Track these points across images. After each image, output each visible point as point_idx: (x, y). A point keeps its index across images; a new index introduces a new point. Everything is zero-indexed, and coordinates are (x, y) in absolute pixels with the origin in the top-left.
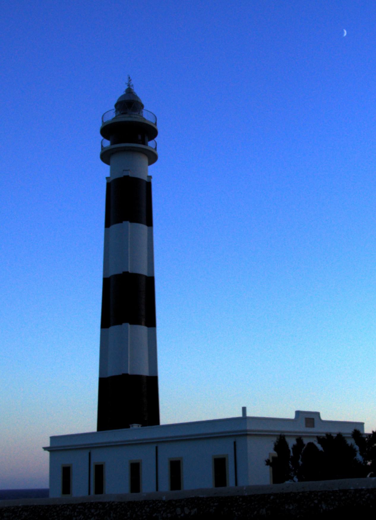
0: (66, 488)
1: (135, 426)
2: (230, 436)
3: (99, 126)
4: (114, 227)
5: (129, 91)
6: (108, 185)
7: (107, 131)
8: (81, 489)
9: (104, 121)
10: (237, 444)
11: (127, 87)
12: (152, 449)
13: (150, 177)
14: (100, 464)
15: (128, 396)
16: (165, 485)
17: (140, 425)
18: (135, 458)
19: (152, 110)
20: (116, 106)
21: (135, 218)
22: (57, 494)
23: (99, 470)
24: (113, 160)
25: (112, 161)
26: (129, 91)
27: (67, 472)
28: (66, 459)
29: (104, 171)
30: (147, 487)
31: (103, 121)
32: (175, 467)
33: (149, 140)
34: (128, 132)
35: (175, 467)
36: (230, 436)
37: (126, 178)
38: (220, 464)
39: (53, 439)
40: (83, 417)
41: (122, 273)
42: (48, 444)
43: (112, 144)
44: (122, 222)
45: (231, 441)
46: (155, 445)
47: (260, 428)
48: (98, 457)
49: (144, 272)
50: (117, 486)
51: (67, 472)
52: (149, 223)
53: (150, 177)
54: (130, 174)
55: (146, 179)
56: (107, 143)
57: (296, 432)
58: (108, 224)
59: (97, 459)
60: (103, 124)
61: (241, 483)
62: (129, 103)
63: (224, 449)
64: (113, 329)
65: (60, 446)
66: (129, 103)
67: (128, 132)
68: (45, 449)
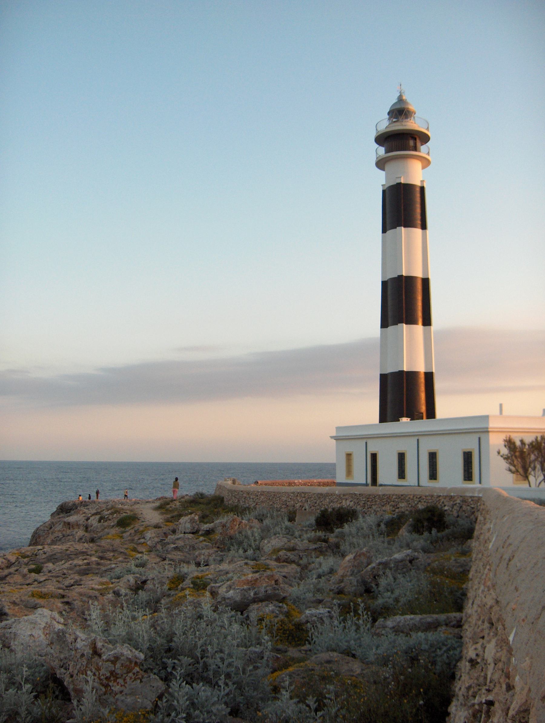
1: (405, 420)
2: (475, 432)
3: (373, 135)
4: (390, 232)
5: (400, 100)
6: (384, 192)
7: (383, 139)
8: (360, 475)
9: (379, 130)
10: (420, 441)
11: (399, 94)
12: (414, 441)
14: (468, 451)
17: (409, 419)
20: (389, 113)
21: (409, 223)
23: (374, 457)
24: (387, 167)
25: (386, 168)
26: (400, 100)
27: (349, 456)
28: (349, 447)
29: (379, 180)
31: (377, 129)
33: (422, 145)
34: (400, 140)
36: (475, 432)
37: (399, 185)
39: (338, 429)
41: (397, 276)
42: (334, 434)
43: (387, 152)
44: (396, 228)
45: (364, 441)
46: (476, 436)
49: (419, 273)
50: (387, 474)
51: (349, 456)
52: (424, 227)
54: (402, 181)
55: (418, 184)
56: (382, 151)
57: (541, 429)
58: (384, 231)
59: (372, 449)
60: (377, 133)
62: (400, 112)
63: (471, 444)
64: (391, 329)
66: (400, 112)
67: (400, 140)
68: (332, 437)
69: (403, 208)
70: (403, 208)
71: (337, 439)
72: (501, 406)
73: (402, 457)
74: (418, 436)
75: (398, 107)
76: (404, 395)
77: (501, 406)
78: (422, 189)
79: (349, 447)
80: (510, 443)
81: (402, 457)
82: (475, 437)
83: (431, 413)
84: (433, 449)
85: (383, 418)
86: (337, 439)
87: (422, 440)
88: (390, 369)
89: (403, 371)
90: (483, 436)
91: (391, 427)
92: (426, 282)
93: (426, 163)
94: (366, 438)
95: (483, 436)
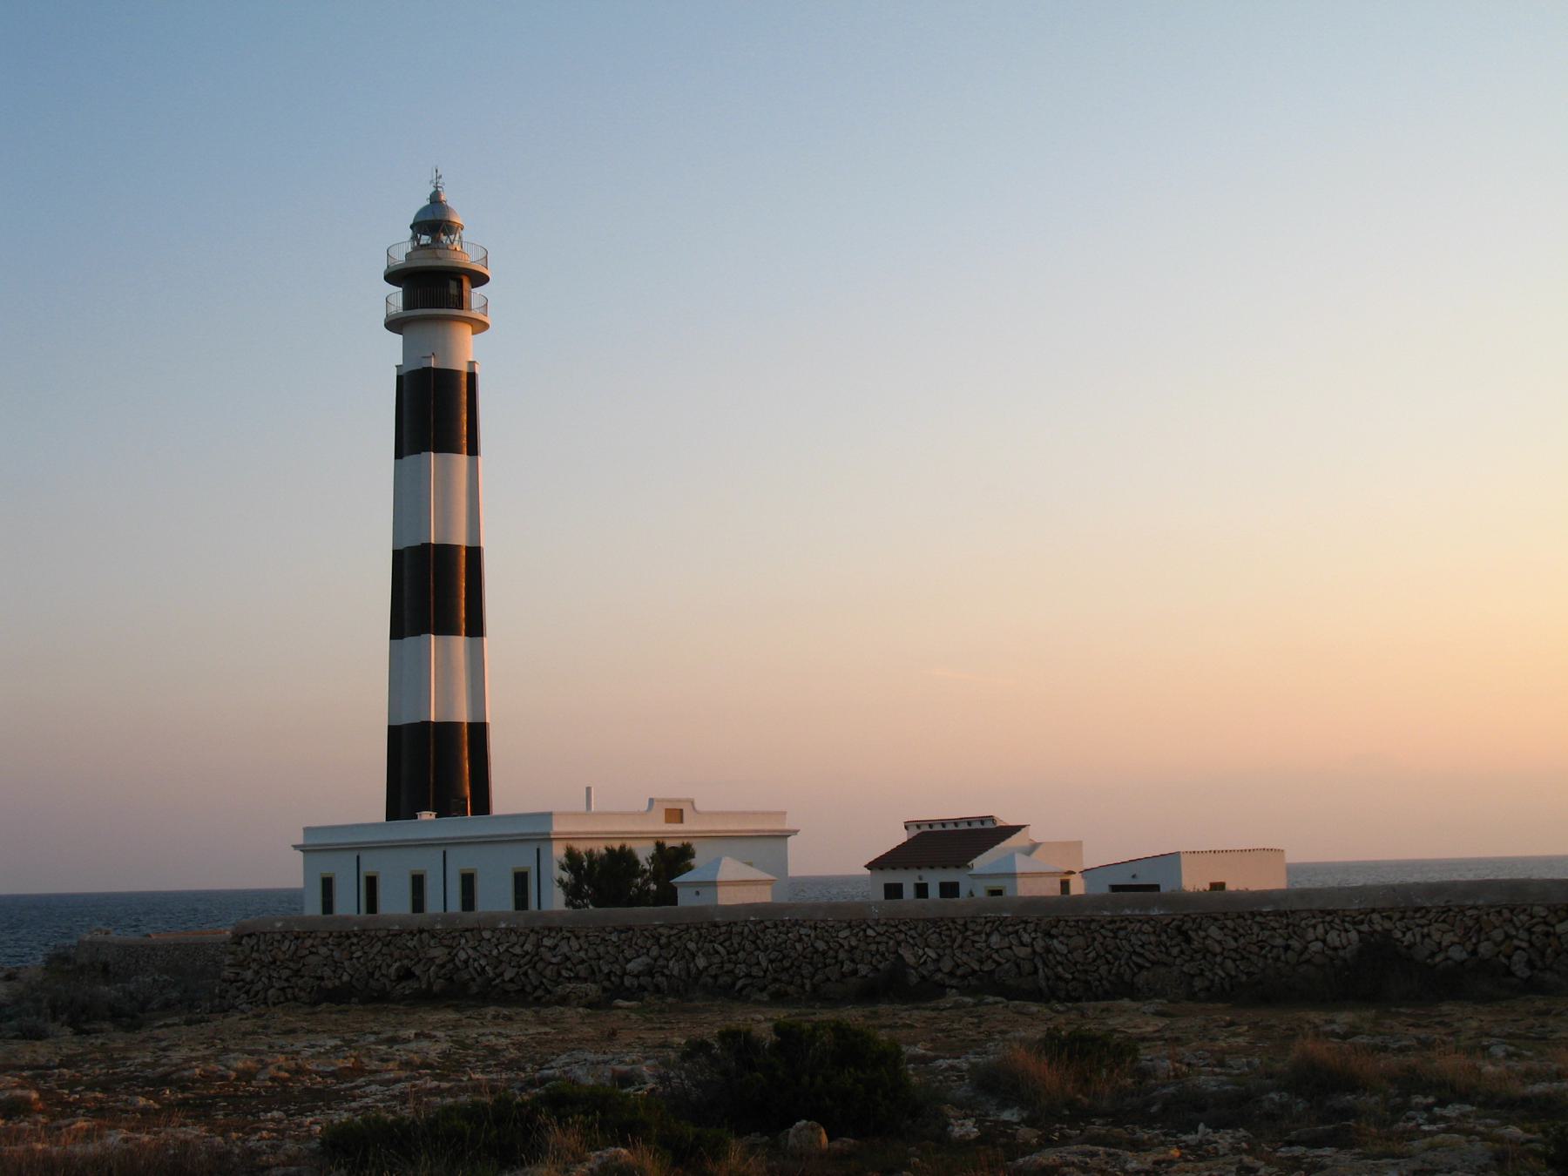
0: (328, 906)
1: (427, 816)
5: (435, 199)
6: (399, 379)
8: (347, 903)
12: (437, 855)
13: (472, 364)
15: (436, 763)
16: (455, 905)
18: (418, 868)
19: (467, 249)
21: (446, 445)
22: (313, 908)
23: (372, 882)
26: (435, 199)
27: (327, 884)
30: (433, 905)
32: (468, 881)
34: (433, 286)
35: (468, 881)
38: (521, 879)
39: (307, 830)
40: (361, 790)
42: (301, 842)
45: (354, 855)
46: (535, 846)
47: (599, 829)
48: (370, 865)
49: (461, 539)
50: (347, 903)
51: (327, 884)
52: (473, 450)
53: (472, 364)
59: (367, 869)
61: (544, 908)
62: (434, 223)
63: (523, 858)
64: (409, 641)
65: (316, 846)
66: (434, 223)
67: (433, 286)
68: (296, 847)
69: (435, 413)
70: (435, 413)
71: (303, 849)
72: (589, 789)
73: (418, 882)
74: (445, 845)
75: (429, 217)
76: (436, 763)
77: (589, 789)
78: (472, 377)
79: (893, 877)
80: (571, 854)
81: (418, 882)
82: (533, 847)
83: (482, 804)
84: (468, 866)
85: (393, 812)
86: (303, 849)
87: (451, 852)
88: (405, 719)
89: (429, 722)
90: (543, 846)
91: (405, 830)
92: (475, 554)
93: (480, 326)
94: (358, 849)
95: (543, 846)
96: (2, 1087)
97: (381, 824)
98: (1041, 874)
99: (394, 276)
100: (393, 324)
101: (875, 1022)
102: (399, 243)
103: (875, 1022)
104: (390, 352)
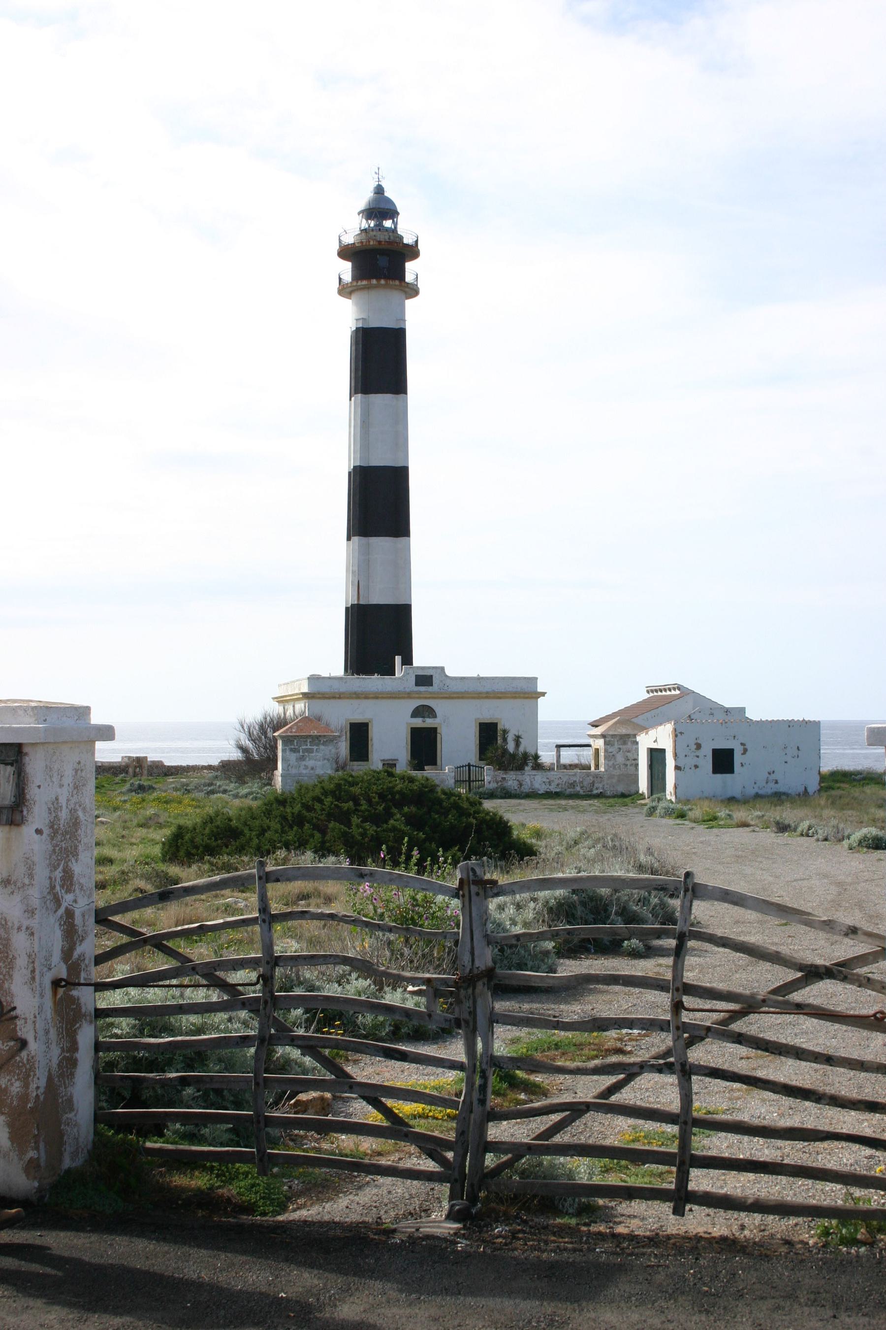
15: (378, 633)
19: (407, 228)
26: (379, 190)
34: (380, 259)
40: (330, 658)
62: (381, 209)
66: (381, 209)
67: (380, 259)
69: (379, 362)
70: (379, 362)
83: (412, 664)
96: (885, 969)
97: (340, 678)
98: (472, 939)
99: (345, 252)
100: (345, 290)
101: (154, 996)
102: (352, 226)
103: (154, 996)
104: (343, 317)
